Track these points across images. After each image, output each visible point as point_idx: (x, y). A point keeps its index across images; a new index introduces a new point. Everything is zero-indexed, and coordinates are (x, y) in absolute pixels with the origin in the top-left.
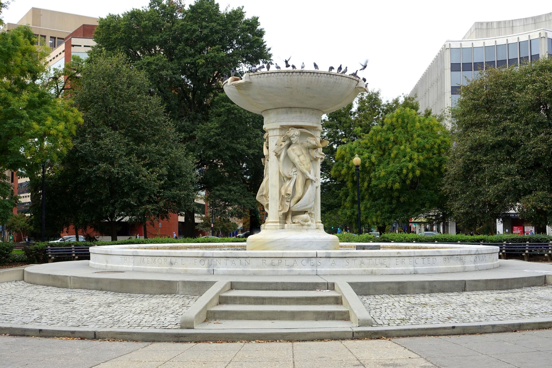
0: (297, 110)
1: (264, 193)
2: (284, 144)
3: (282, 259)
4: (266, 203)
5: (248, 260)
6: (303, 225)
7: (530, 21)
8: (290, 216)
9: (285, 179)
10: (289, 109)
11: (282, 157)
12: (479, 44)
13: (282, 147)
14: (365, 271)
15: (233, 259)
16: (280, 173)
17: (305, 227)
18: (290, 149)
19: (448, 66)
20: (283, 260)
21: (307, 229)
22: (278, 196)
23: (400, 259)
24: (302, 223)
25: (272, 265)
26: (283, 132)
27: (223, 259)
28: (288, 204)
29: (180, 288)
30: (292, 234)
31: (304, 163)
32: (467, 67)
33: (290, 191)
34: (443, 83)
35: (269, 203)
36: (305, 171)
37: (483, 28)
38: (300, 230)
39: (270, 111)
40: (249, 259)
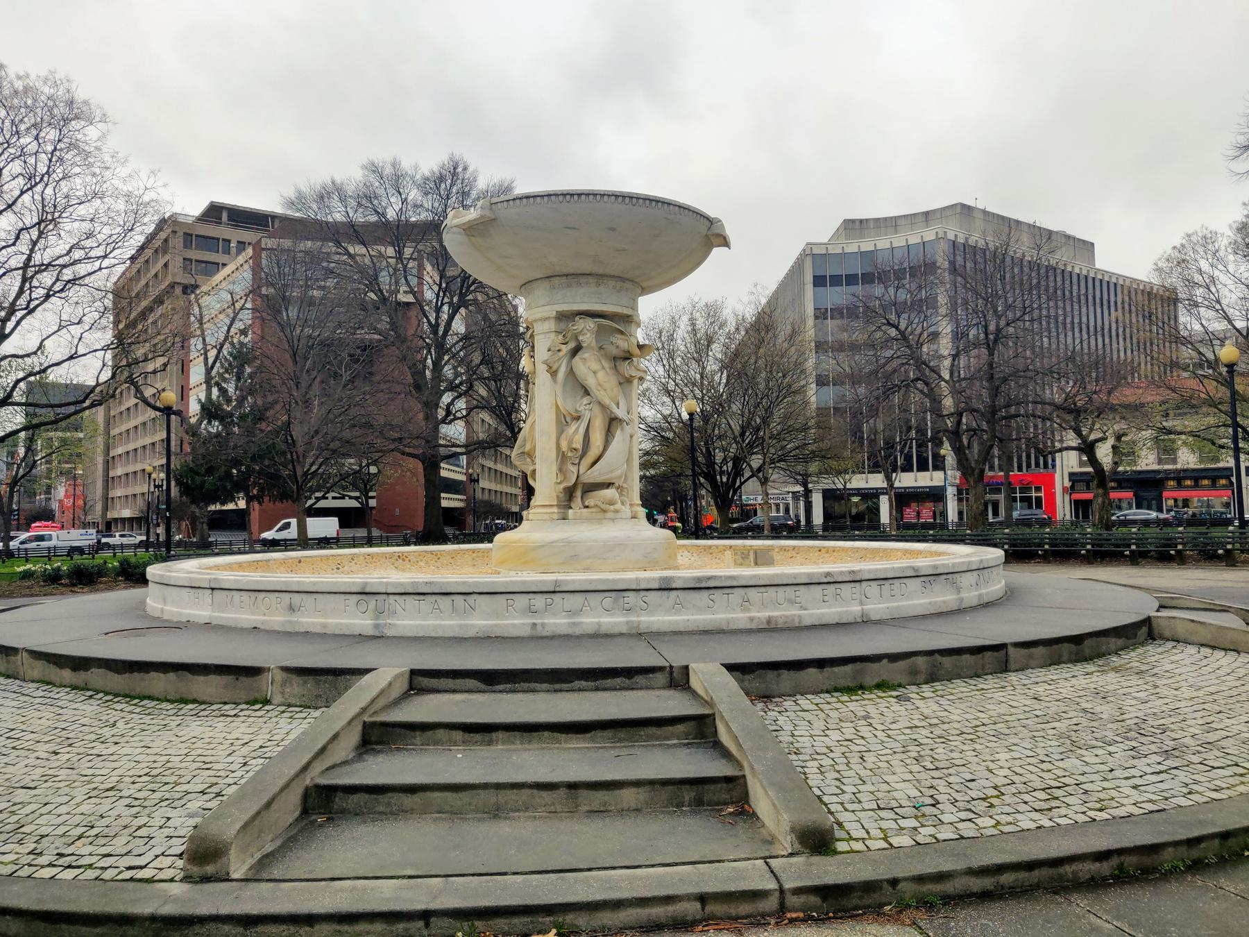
0: (591, 280)
1: (527, 449)
2: (565, 349)
3: (552, 596)
4: (531, 468)
5: (471, 599)
6: (604, 511)
7: (921, 219)
8: (579, 493)
9: (568, 419)
10: (573, 277)
11: (561, 375)
12: (852, 248)
13: (561, 354)
14: (752, 619)
15: (434, 597)
16: (557, 407)
17: (610, 515)
18: (577, 358)
19: (809, 279)
20: (556, 597)
21: (613, 520)
22: (553, 454)
23: (832, 587)
24: (604, 507)
25: (531, 611)
26: (562, 326)
27: (409, 599)
28: (574, 469)
29: (269, 685)
30: (583, 531)
31: (607, 386)
32: (836, 281)
33: (578, 444)
34: (802, 305)
35: (537, 467)
36: (607, 401)
37: (853, 227)
38: (600, 521)
39: (535, 284)
40: (475, 596)
